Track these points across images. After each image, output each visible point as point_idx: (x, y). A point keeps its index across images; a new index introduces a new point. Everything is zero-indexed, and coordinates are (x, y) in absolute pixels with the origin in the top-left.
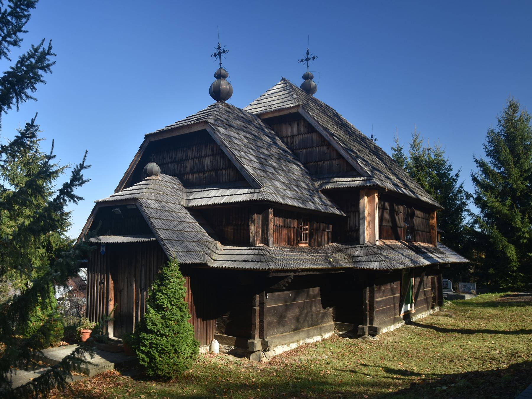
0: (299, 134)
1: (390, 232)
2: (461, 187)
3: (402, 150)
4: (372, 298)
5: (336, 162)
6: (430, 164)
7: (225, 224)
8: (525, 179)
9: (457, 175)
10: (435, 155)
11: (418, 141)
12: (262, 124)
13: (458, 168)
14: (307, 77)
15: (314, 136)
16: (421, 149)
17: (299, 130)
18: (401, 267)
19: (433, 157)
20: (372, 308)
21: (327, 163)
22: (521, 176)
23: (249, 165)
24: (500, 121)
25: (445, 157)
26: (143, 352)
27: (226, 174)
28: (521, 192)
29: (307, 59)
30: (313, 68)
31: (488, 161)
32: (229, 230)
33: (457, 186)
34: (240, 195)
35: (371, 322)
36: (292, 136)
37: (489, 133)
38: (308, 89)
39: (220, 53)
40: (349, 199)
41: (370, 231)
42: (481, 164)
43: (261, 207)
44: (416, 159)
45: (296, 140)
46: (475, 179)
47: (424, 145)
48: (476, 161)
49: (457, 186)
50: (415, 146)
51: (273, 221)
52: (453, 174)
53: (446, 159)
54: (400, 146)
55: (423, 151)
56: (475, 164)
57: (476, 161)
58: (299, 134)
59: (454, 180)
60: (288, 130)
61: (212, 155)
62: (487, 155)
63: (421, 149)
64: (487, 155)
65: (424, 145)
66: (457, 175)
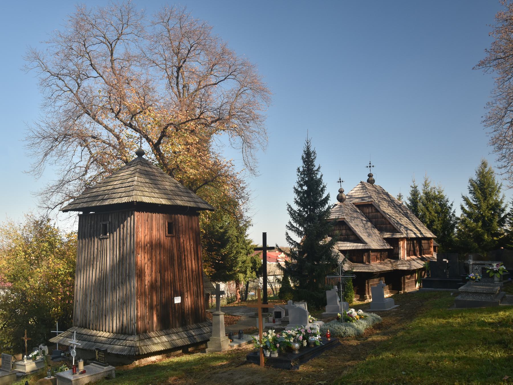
0: (372, 212)
1: (413, 253)
2: (454, 212)
3: (417, 188)
4: (404, 280)
5: (388, 226)
6: (435, 198)
7: (354, 256)
8: (490, 210)
9: (452, 205)
10: (438, 192)
11: (427, 182)
12: (355, 207)
13: (453, 200)
14: (370, 176)
15: (379, 214)
16: (430, 188)
17: (372, 211)
18: (416, 268)
19: (437, 193)
20: (404, 285)
21: (384, 226)
22: (487, 208)
23: (364, 236)
24: (477, 172)
25: (444, 194)
26: (37, 355)
27: (352, 237)
28: (488, 217)
29: (370, 167)
30: (373, 171)
31: (470, 196)
32: (355, 258)
33: (452, 211)
34: (360, 246)
35: (404, 290)
36: (369, 213)
37: (470, 180)
38: (371, 181)
39: (340, 181)
40: (394, 242)
41: (403, 253)
42: (466, 199)
43: (368, 251)
44: (427, 194)
45: (371, 214)
46: (462, 208)
47: (431, 185)
48: (463, 197)
49: (452, 211)
50: (426, 185)
51: (372, 254)
52: (449, 204)
53: (444, 195)
54: (416, 185)
55: (431, 189)
56: (463, 199)
57: (463, 197)
58: (372, 212)
59: (450, 208)
60: (367, 210)
61: (346, 230)
62: (470, 193)
63: (430, 188)
64: (470, 193)
65: (431, 185)
66: (452, 205)
